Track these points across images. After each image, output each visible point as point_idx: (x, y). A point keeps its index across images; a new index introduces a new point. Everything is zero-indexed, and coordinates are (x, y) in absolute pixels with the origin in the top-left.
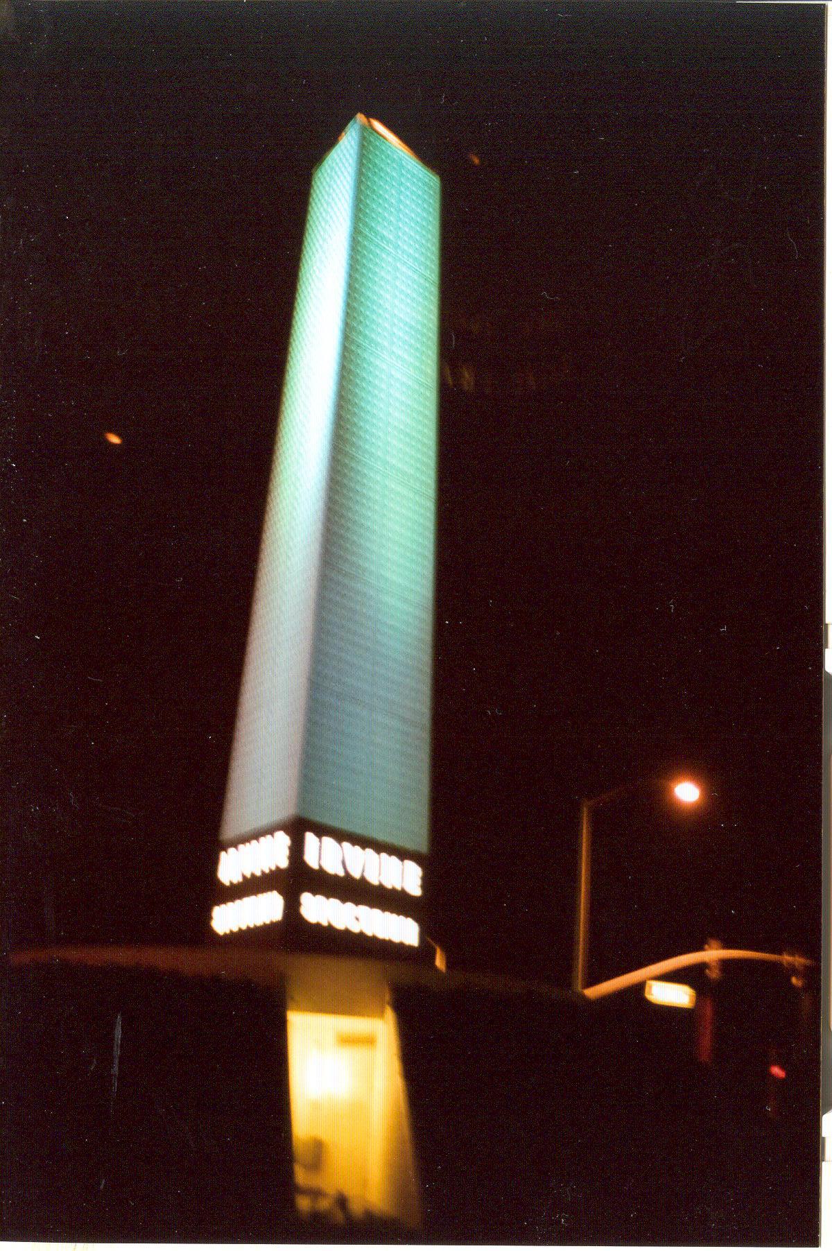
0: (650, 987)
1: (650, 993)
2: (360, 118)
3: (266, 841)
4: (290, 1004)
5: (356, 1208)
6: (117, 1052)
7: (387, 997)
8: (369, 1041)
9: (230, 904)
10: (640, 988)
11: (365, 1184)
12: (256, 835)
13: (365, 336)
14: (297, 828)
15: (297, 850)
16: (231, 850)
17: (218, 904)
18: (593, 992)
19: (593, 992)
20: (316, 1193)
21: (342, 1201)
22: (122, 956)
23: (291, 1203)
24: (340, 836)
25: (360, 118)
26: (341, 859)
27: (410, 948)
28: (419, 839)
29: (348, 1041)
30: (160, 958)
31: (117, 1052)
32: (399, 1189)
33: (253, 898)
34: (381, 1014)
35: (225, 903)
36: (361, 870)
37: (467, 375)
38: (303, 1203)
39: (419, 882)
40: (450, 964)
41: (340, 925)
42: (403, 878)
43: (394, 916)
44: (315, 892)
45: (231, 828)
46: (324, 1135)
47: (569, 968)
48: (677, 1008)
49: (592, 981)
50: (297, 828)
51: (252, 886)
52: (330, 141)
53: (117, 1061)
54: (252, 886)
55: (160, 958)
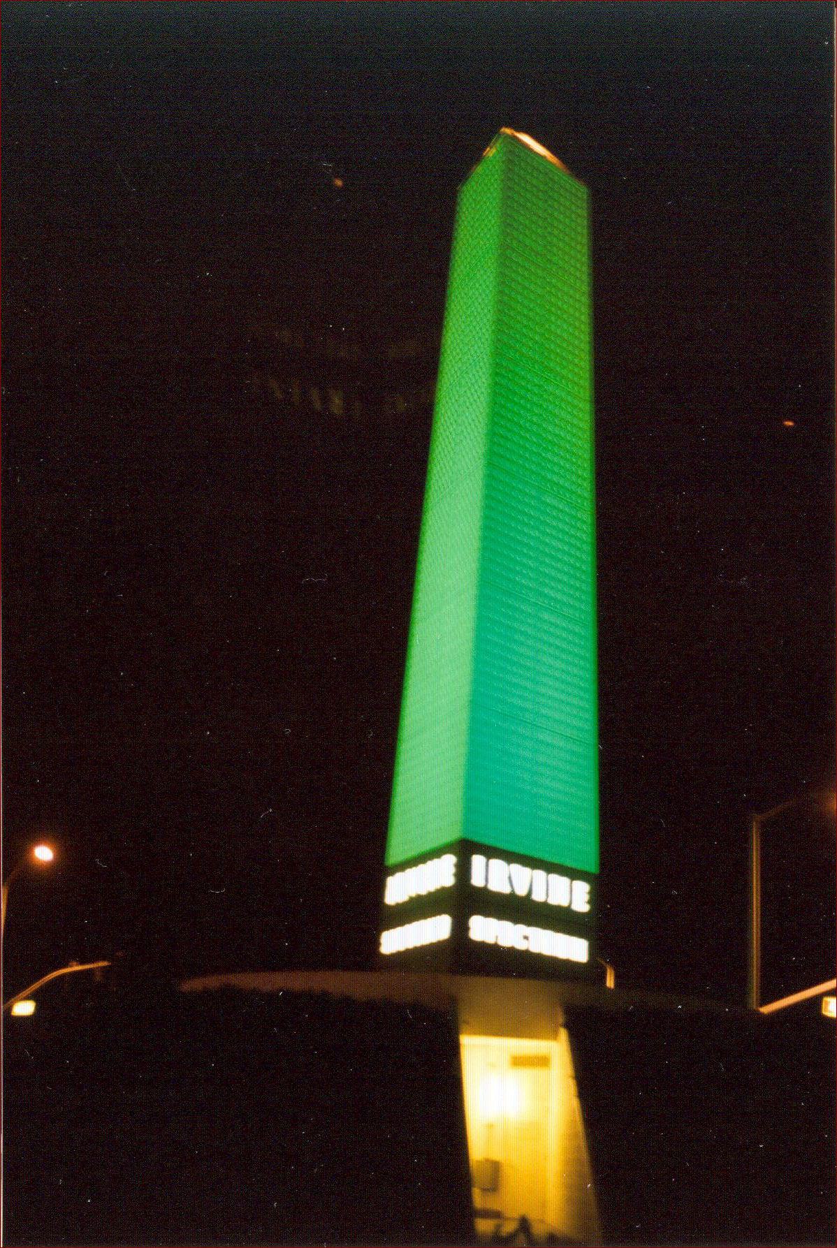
0: (827, 1003)
4: (464, 1027)
5: (539, 1230)
7: (561, 1019)
8: (542, 1061)
10: (816, 1002)
11: (544, 1205)
14: (465, 850)
15: (463, 870)
16: (399, 875)
17: (388, 928)
18: (766, 1010)
19: (766, 1010)
20: (497, 1215)
21: (524, 1224)
22: (297, 981)
23: (471, 1228)
24: (510, 857)
26: (507, 876)
28: (592, 866)
29: (519, 1061)
30: (36, 986)
32: (575, 1201)
34: (554, 1036)
36: (528, 885)
37: (337, 401)
38: (484, 1226)
39: (587, 897)
40: (617, 984)
42: (571, 894)
44: (486, 914)
45: (395, 853)
46: (496, 1156)
47: (744, 981)
49: (765, 1001)
50: (465, 850)
52: (475, 156)
55: (36, 986)
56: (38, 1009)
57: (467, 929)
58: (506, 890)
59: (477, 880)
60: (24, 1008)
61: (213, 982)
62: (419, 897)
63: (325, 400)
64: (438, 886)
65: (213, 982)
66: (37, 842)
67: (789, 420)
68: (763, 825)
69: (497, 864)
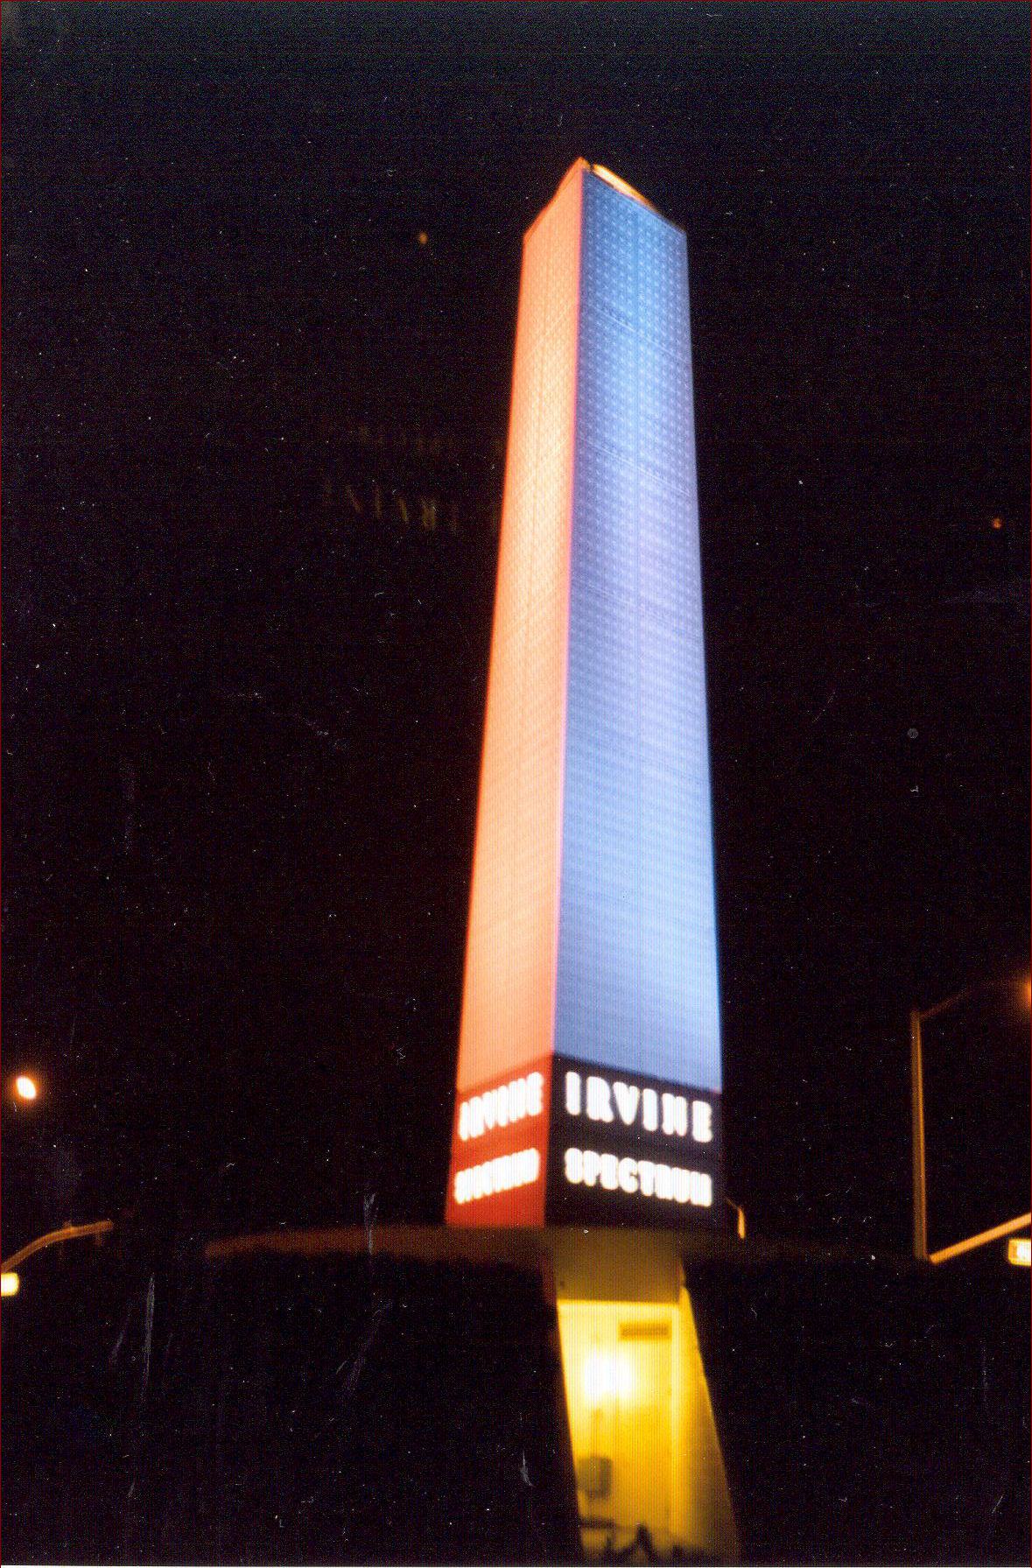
0: (1015, 1248)
1: (1015, 1256)
3: (518, 1086)
7: (682, 1277)
8: (659, 1331)
9: (477, 1168)
10: (1001, 1245)
13: (605, 441)
16: (475, 1101)
18: (937, 1258)
19: (937, 1258)
24: (612, 1075)
25: (581, 164)
27: (700, 1209)
29: (631, 1332)
32: (705, 1502)
33: (506, 1159)
41: (609, 1184)
43: (686, 1172)
46: (606, 1450)
51: (499, 1142)
52: (544, 195)
54: (499, 1142)
58: (608, 1117)
59: (573, 1107)
64: (522, 1115)
69: (597, 1085)
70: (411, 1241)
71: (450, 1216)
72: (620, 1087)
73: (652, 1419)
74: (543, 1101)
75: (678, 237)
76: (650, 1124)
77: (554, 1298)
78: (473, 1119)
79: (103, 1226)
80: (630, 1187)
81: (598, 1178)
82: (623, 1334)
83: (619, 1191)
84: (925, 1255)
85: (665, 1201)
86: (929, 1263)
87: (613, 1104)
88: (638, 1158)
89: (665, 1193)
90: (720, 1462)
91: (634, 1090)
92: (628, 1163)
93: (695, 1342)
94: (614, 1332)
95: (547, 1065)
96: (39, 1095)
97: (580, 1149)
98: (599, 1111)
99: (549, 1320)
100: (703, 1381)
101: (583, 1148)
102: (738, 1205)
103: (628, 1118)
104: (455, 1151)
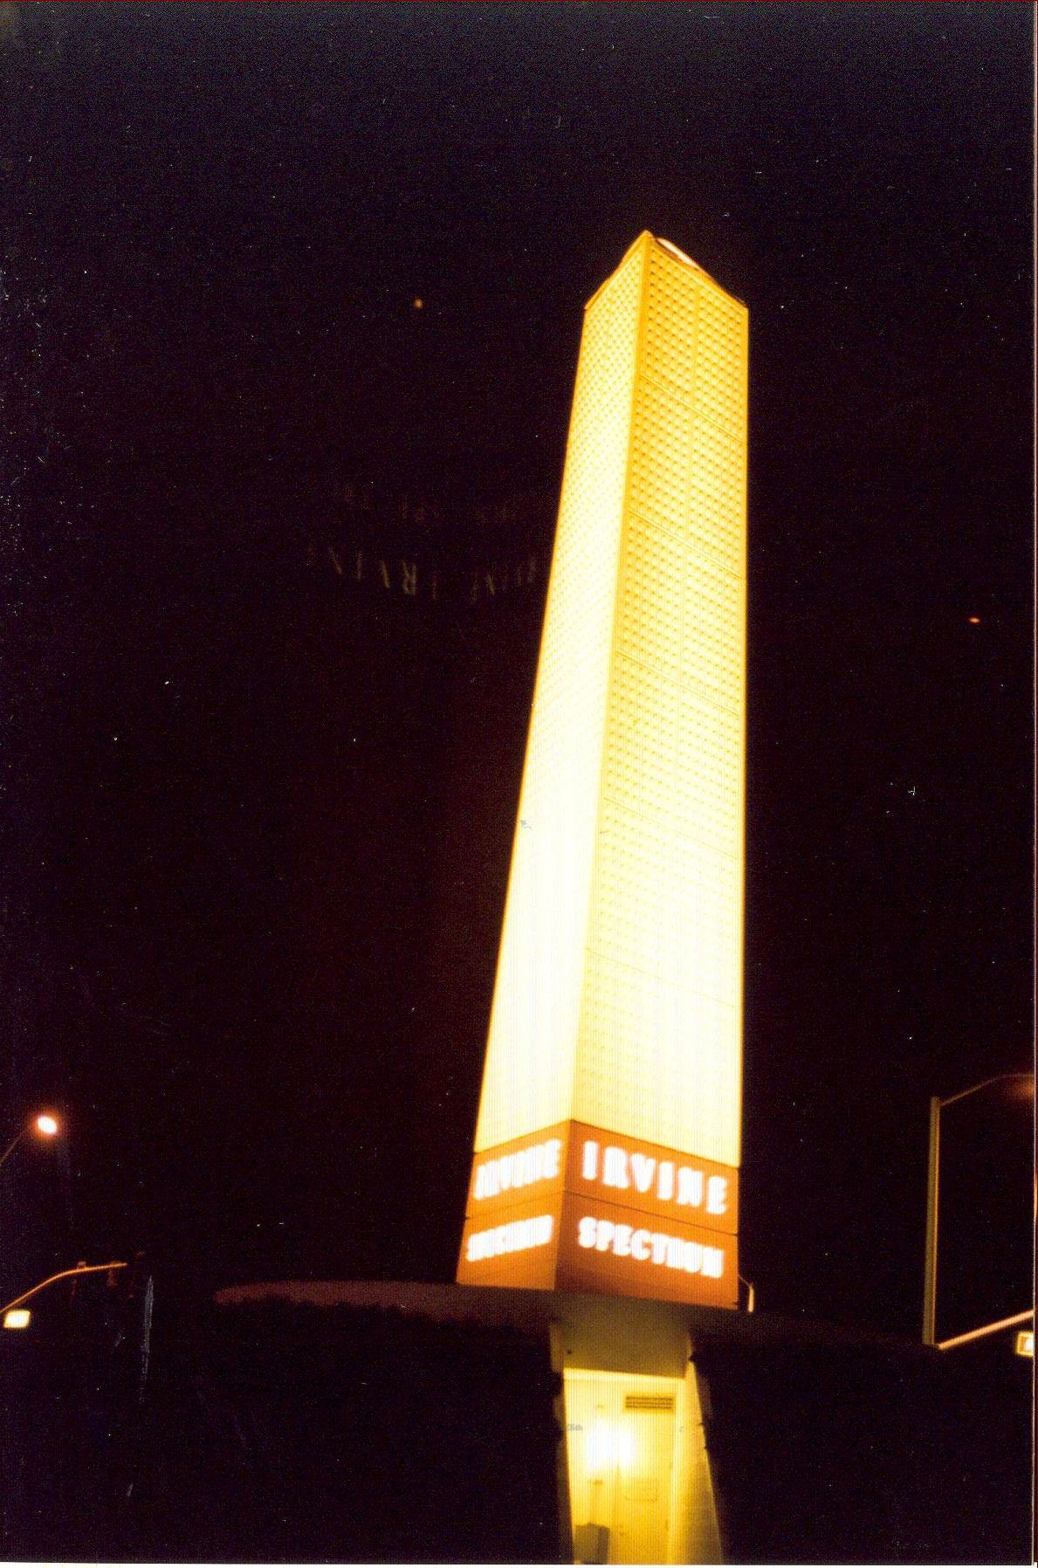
0: (1024, 1340)
1: (1022, 1349)
2: (646, 235)
3: (538, 1150)
6: (148, 1324)
8: (664, 1404)
10: (1011, 1333)
12: (519, 1144)
16: (491, 1164)
18: (943, 1346)
19: (943, 1346)
24: (632, 1145)
25: (646, 235)
29: (634, 1403)
30: (409, 1296)
31: (148, 1324)
34: (682, 1373)
35: (706, 1448)
41: (621, 1250)
46: (604, 1520)
48: (555, 527)
49: (941, 1337)
53: (147, 1335)
54: (514, 1206)
56: (33, 1320)
57: (576, 1233)
58: (623, 1184)
59: (589, 1173)
60: (18, 1319)
61: (256, 1292)
62: (513, 1191)
63: (396, 577)
64: (537, 1177)
65: (256, 1292)
66: (38, 1111)
67: (976, 617)
68: (943, 1111)
69: (614, 1156)
70: (409, 1296)
71: (463, 1277)
72: (638, 1159)
73: (652, 1492)
74: (559, 1164)
75: (745, 312)
76: (665, 1194)
77: (562, 1367)
78: (486, 1182)
79: (125, 1264)
80: (641, 1255)
81: (611, 1244)
82: (627, 1407)
83: (629, 1258)
84: (933, 1343)
85: (673, 1271)
86: (936, 1350)
87: (630, 1171)
88: (653, 1230)
89: (674, 1263)
90: (714, 1521)
91: (652, 1162)
92: (643, 1235)
93: (703, 1442)
94: (620, 1402)
95: (565, 1133)
96: (59, 1131)
97: (473, 1157)
98: (615, 1177)
99: (555, 1386)
100: (704, 1457)
101: (599, 1217)
102: (749, 1282)
103: (643, 1186)
104: (470, 1211)
